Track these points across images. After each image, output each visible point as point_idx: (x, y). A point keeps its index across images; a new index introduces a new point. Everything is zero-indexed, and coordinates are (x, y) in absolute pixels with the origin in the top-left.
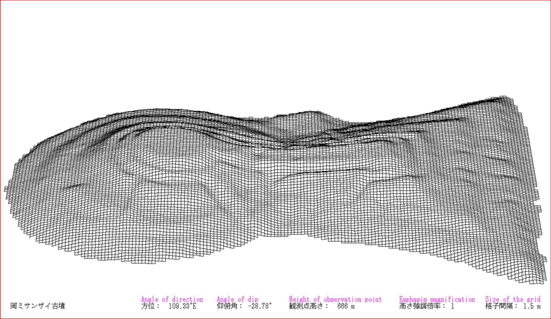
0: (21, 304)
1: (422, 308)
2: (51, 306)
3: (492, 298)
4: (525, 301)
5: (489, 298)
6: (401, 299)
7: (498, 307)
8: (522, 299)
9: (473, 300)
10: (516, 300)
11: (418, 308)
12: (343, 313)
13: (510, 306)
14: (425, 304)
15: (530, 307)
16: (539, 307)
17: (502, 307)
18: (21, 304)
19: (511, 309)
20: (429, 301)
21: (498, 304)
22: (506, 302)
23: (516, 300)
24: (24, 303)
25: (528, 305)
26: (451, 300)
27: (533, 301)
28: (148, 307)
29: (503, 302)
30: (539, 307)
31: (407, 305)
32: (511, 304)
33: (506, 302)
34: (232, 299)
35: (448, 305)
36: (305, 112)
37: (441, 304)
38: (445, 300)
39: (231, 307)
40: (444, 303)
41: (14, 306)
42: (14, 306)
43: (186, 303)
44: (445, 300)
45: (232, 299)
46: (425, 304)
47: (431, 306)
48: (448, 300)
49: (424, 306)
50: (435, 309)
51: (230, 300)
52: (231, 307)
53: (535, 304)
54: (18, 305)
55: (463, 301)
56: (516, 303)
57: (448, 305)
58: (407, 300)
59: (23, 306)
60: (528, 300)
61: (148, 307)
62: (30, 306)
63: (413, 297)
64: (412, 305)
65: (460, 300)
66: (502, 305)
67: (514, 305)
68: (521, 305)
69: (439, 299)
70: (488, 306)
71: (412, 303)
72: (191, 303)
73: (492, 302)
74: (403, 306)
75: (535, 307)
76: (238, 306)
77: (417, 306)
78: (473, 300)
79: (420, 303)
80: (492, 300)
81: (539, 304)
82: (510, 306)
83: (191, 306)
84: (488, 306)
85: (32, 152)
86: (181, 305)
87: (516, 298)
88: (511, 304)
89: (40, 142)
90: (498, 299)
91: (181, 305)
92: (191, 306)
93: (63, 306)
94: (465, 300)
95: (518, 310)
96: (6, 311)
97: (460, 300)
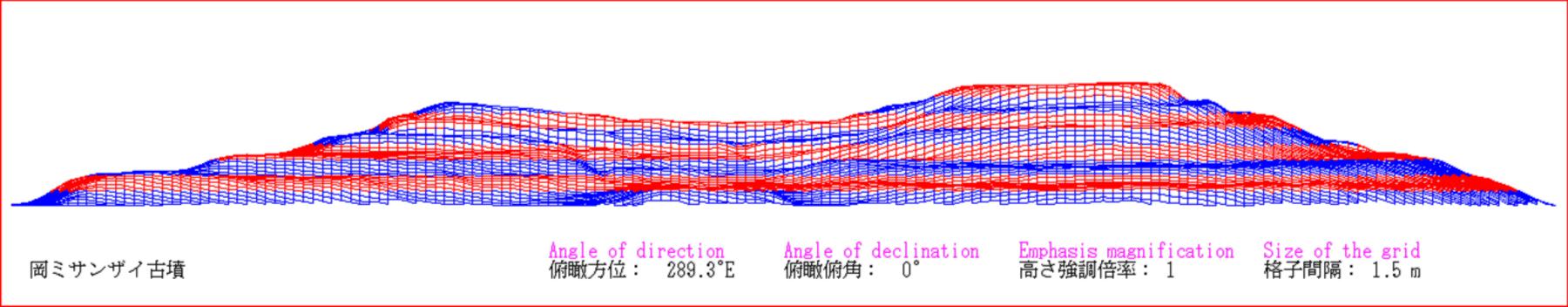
0: (59, 264)
1: (1083, 276)
2: (145, 271)
3: (1282, 248)
4: (1377, 255)
5: (1274, 248)
6: (1022, 250)
7: (1299, 274)
8: (1367, 251)
9: (1227, 253)
10: (1350, 251)
11: (1073, 274)
12: (684, 290)
13: (1335, 270)
14: (1091, 265)
15: (1391, 273)
16: (1416, 272)
17: (1312, 272)
18: (59, 264)
19: (1335, 279)
20: (1102, 256)
21: (1301, 265)
22: (1323, 259)
23: (1350, 251)
24: (67, 263)
25: (1385, 267)
26: (1166, 252)
27: (1400, 255)
28: (607, 272)
29: (1314, 259)
30: (1416, 272)
31: (1040, 268)
32: (1336, 264)
33: (1323, 259)
34: (593, 251)
35: (1158, 266)
36: (977, 87)
37: (1139, 266)
38: (1147, 254)
39: (844, 271)
40: (1147, 260)
41: (39, 269)
42: (39, 269)
43: (677, 260)
44: (1147, 254)
45: (593, 251)
46: (1091, 265)
47: (1109, 269)
48: (1156, 253)
49: (1089, 270)
50: (1119, 279)
51: (586, 254)
52: (844, 271)
53: (1405, 266)
54: (51, 268)
55: (1201, 256)
56: (1351, 261)
57: (1158, 266)
58: (1040, 252)
59: (66, 270)
60: (1386, 253)
61: (607, 272)
62: (87, 271)
63: (1056, 245)
64: (1056, 268)
65: (1190, 253)
66: (1311, 268)
67: (1344, 268)
68: (1364, 267)
69: (1131, 251)
70: (1272, 269)
71: (1055, 261)
72: (720, 263)
73: (1283, 260)
74: (1028, 269)
75: (1406, 272)
76: (865, 270)
77: (1070, 271)
78: (1227, 253)
79: (1078, 260)
80: (1283, 253)
81: (1415, 263)
82: (1335, 270)
83: (720, 270)
84: (1272, 269)
85: (1240, 118)
86: (702, 268)
87: (1351, 247)
88: (1336, 264)
89: (1258, 111)
90: (1299, 251)
91: (702, 268)
92: (720, 270)
93: (178, 269)
94: (950, 251)
95: (1356, 284)
96: (19, 287)
97: (1190, 253)
